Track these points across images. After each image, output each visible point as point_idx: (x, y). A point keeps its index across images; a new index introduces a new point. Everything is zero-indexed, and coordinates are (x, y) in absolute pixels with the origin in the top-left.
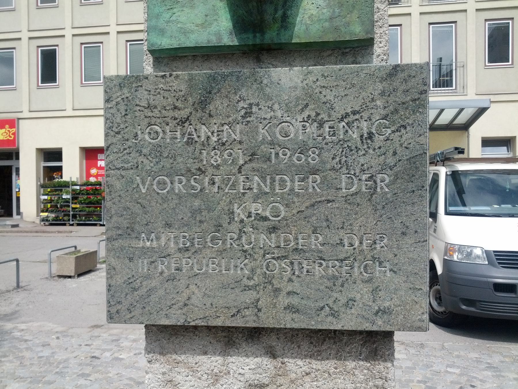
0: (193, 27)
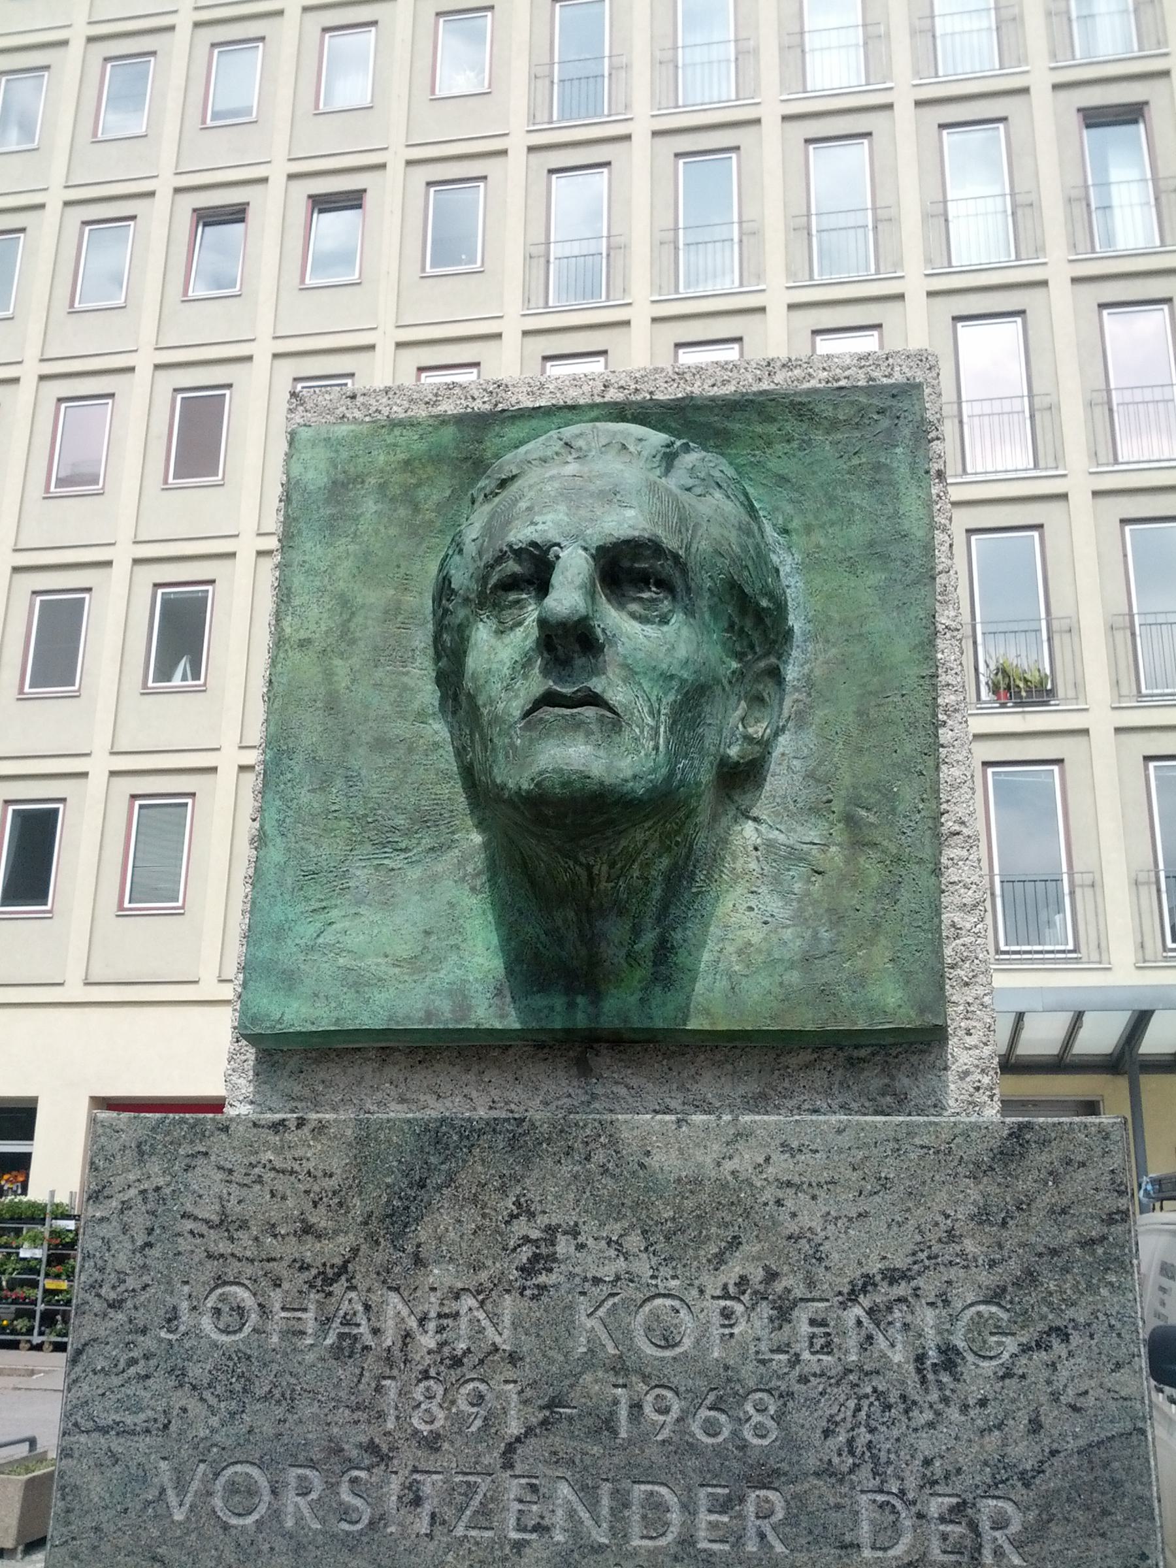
0: (383, 968)
